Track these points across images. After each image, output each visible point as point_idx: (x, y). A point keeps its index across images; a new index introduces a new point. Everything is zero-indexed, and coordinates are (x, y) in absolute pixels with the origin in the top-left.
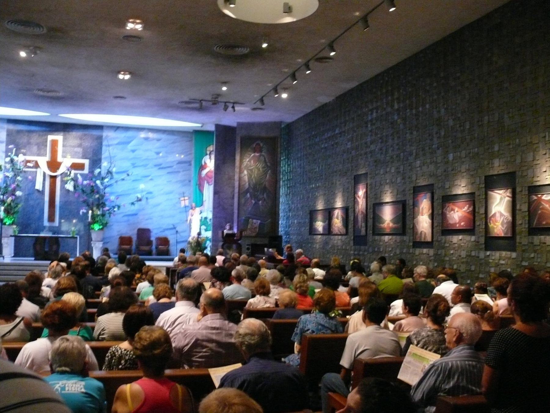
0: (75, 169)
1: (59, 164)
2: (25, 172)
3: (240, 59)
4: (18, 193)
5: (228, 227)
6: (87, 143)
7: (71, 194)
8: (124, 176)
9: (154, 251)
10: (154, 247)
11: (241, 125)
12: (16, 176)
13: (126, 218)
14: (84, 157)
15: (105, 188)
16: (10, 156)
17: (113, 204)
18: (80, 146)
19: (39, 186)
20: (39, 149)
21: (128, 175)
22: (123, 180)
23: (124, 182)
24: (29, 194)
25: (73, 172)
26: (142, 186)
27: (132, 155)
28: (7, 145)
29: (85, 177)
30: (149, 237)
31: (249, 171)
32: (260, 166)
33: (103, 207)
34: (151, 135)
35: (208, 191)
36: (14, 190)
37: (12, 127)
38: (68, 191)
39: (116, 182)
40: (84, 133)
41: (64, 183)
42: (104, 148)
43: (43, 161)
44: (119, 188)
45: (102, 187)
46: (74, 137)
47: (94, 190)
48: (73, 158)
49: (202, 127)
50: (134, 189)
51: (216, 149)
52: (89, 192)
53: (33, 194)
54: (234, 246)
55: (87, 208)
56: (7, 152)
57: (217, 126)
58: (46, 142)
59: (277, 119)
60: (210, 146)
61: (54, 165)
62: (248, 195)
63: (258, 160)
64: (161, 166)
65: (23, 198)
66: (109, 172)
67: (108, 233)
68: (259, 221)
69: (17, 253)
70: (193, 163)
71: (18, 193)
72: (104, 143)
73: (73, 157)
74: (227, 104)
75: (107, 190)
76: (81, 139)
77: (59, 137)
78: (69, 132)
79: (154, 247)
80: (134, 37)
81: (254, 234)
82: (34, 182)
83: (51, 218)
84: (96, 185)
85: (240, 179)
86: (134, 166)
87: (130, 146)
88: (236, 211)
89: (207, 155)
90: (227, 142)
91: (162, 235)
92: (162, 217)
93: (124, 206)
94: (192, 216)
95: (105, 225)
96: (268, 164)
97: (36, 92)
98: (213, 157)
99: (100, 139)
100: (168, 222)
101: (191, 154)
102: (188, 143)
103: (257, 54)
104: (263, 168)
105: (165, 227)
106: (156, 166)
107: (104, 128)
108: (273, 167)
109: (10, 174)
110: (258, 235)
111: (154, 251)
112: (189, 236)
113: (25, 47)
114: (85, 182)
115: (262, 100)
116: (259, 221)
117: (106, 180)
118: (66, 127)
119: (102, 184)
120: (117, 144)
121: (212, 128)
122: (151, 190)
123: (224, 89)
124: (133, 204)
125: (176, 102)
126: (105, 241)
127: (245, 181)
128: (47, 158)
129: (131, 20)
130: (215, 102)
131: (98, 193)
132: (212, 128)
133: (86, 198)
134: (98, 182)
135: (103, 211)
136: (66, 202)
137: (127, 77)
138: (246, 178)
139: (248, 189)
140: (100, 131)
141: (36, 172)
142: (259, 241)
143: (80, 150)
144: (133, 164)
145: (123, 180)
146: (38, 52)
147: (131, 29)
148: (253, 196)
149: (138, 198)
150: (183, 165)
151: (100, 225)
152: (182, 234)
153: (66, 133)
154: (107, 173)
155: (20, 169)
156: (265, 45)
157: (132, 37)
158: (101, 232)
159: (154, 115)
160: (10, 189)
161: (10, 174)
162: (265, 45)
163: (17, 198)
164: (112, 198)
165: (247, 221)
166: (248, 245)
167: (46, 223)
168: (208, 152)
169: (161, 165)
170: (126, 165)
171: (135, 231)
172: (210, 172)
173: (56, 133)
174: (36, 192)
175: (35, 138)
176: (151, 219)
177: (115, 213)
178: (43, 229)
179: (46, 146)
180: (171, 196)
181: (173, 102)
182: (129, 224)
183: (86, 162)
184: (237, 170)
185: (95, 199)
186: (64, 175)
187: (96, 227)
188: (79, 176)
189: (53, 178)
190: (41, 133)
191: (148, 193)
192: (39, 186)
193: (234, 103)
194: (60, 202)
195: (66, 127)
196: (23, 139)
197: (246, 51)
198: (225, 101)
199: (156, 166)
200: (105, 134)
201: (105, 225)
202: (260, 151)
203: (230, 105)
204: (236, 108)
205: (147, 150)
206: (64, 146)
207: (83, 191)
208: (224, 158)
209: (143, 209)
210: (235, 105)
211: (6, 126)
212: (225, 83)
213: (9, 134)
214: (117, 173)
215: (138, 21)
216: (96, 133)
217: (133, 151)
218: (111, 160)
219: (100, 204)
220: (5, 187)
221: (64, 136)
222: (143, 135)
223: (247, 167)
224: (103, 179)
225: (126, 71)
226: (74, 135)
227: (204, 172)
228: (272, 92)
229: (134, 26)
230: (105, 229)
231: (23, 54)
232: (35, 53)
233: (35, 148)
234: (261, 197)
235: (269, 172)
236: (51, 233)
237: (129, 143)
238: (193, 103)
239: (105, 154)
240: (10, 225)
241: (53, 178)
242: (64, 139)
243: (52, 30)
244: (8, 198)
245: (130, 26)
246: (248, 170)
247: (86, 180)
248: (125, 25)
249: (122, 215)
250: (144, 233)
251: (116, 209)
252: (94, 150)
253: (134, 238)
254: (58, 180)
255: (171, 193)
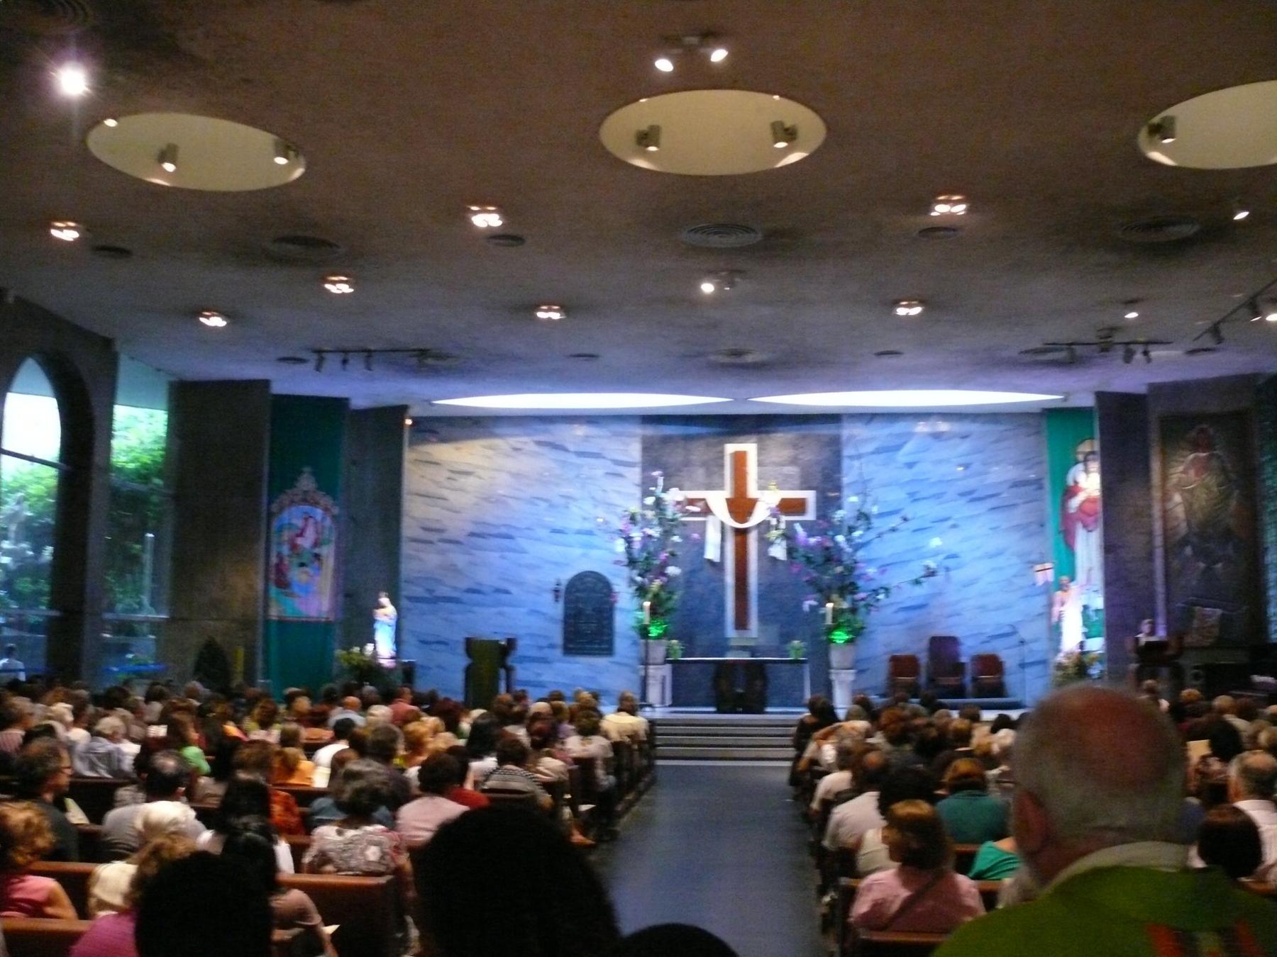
0: (787, 514)
1: (753, 502)
2: (685, 524)
3: (1180, 247)
4: (672, 570)
5: (1145, 627)
6: (810, 455)
7: (781, 567)
8: (895, 521)
9: (970, 687)
10: (968, 679)
11: (1156, 389)
12: (667, 533)
13: (901, 616)
14: (805, 486)
15: (856, 550)
16: (652, 494)
17: (874, 586)
18: (793, 461)
19: (712, 553)
20: (709, 474)
21: (905, 520)
22: (893, 530)
23: (894, 535)
24: (693, 572)
25: (784, 518)
26: (936, 542)
27: (908, 474)
28: (644, 470)
29: (809, 528)
30: (957, 655)
31: (1186, 495)
32: (1211, 480)
33: (853, 593)
34: (943, 427)
35: (1088, 548)
36: (665, 564)
37: (651, 431)
38: (774, 559)
39: (880, 536)
40: (803, 432)
41: (765, 543)
42: (846, 463)
43: (718, 500)
44: (884, 549)
45: (849, 550)
46: (781, 443)
47: (830, 556)
48: (782, 489)
49: (1065, 400)
50: (917, 549)
51: (1103, 448)
52: (820, 560)
53: (701, 570)
54: (1165, 671)
55: (817, 595)
56: (646, 487)
57: (1100, 396)
58: (722, 458)
59: (1248, 370)
60: (1082, 442)
61: (741, 506)
62: (1188, 550)
63: (1203, 467)
64: (974, 496)
65: (681, 580)
66: (864, 516)
67: (864, 648)
68: (1219, 611)
69: (678, 700)
70: (1047, 484)
71: (672, 570)
72: (847, 451)
73: (781, 487)
74: (1132, 346)
75: (860, 554)
76: (795, 446)
77: (749, 448)
78: (767, 432)
79: (968, 679)
80: (946, 229)
81: (1207, 642)
82: (701, 545)
83: (741, 623)
84: (836, 543)
85: (1165, 514)
86: (914, 498)
87: (902, 456)
88: (1160, 589)
89: (1077, 462)
90: (1126, 432)
91: (987, 649)
92: (983, 608)
93: (898, 587)
94: (1063, 604)
95: (857, 633)
96: (1233, 476)
97: (712, 358)
98: (1095, 466)
99: (835, 444)
100: (994, 621)
101: (1039, 463)
102: (1032, 438)
103: (1218, 232)
104: (1219, 485)
105: (990, 631)
106: (962, 495)
107: (844, 418)
108: (1244, 480)
109: (655, 532)
110: (1221, 643)
111: (970, 687)
112: (1058, 651)
113: (710, 274)
114: (813, 540)
115: (1215, 331)
116: (1219, 611)
117: (857, 534)
118: (759, 424)
119: (849, 540)
120: (873, 453)
121: (1088, 401)
122: (955, 550)
123: (1132, 315)
124: (917, 582)
125: (1013, 353)
126: (864, 666)
127: (1177, 518)
128: (727, 493)
129: (942, 198)
130: (1108, 343)
131: (840, 562)
132: (1088, 401)
133: (815, 575)
134: (840, 538)
135: (854, 601)
136: (771, 585)
137: (916, 311)
138: (1180, 512)
139: (1187, 535)
140: (833, 426)
141: (704, 523)
142: (1225, 659)
143: (792, 470)
144: (911, 494)
145: (893, 530)
146: (737, 280)
147: (943, 215)
148: (1200, 553)
149: (928, 568)
150: (1023, 489)
151: (848, 633)
152: (1035, 646)
153: (763, 436)
154: (858, 518)
155: (672, 520)
156: (1242, 216)
157: (947, 228)
158: (851, 648)
159: (957, 384)
160: (657, 562)
161: (655, 532)
162: (1242, 216)
163: (671, 579)
164: (871, 571)
165: (1188, 613)
166: (1197, 668)
167: (731, 632)
168: (1081, 457)
169: (971, 493)
170: (895, 497)
171: (924, 644)
172: (1089, 500)
173: (742, 438)
174: (707, 566)
175: (699, 452)
176: (959, 615)
177: (880, 604)
178: (723, 647)
179: (722, 466)
180: (1001, 561)
181: (1005, 354)
182: (910, 629)
183: (810, 496)
184: (1157, 494)
185: (835, 575)
186: (764, 526)
187: (840, 637)
188: (799, 528)
189: (741, 534)
190: (712, 440)
191: (948, 557)
192: (712, 553)
193: (1147, 343)
194: (760, 584)
195: (759, 424)
196: (675, 456)
197: (1188, 230)
198: (1127, 340)
199: (962, 495)
200: (848, 431)
201: (857, 633)
202: (1208, 446)
203: (1140, 349)
204: (1153, 354)
205: (940, 462)
206: (760, 464)
207: (809, 560)
208: (1123, 470)
209: (940, 594)
210: (1150, 347)
211: (639, 430)
212: (1131, 304)
213: (648, 446)
214: (881, 515)
215: (956, 198)
216: (826, 430)
217: (910, 465)
218: (863, 488)
219: (847, 587)
220: (647, 558)
221: (758, 442)
222: (922, 428)
223: (1180, 487)
224: (851, 529)
225: (912, 300)
226: (781, 440)
227: (1075, 503)
228: (1244, 311)
229: (948, 209)
230: (860, 641)
231: (708, 288)
232: (732, 284)
233: (700, 473)
234: (1220, 553)
235: (1236, 493)
236: (747, 653)
237: (898, 448)
238: (1056, 350)
239: (848, 476)
240: (659, 637)
241: (741, 534)
242: (761, 450)
243: (772, 234)
244: (651, 581)
245: (940, 209)
246: (1182, 492)
247: (813, 536)
248: (928, 207)
249: (894, 608)
250: (943, 647)
251: (881, 597)
252: (824, 469)
253: (924, 659)
254: (753, 540)
255: (999, 553)
